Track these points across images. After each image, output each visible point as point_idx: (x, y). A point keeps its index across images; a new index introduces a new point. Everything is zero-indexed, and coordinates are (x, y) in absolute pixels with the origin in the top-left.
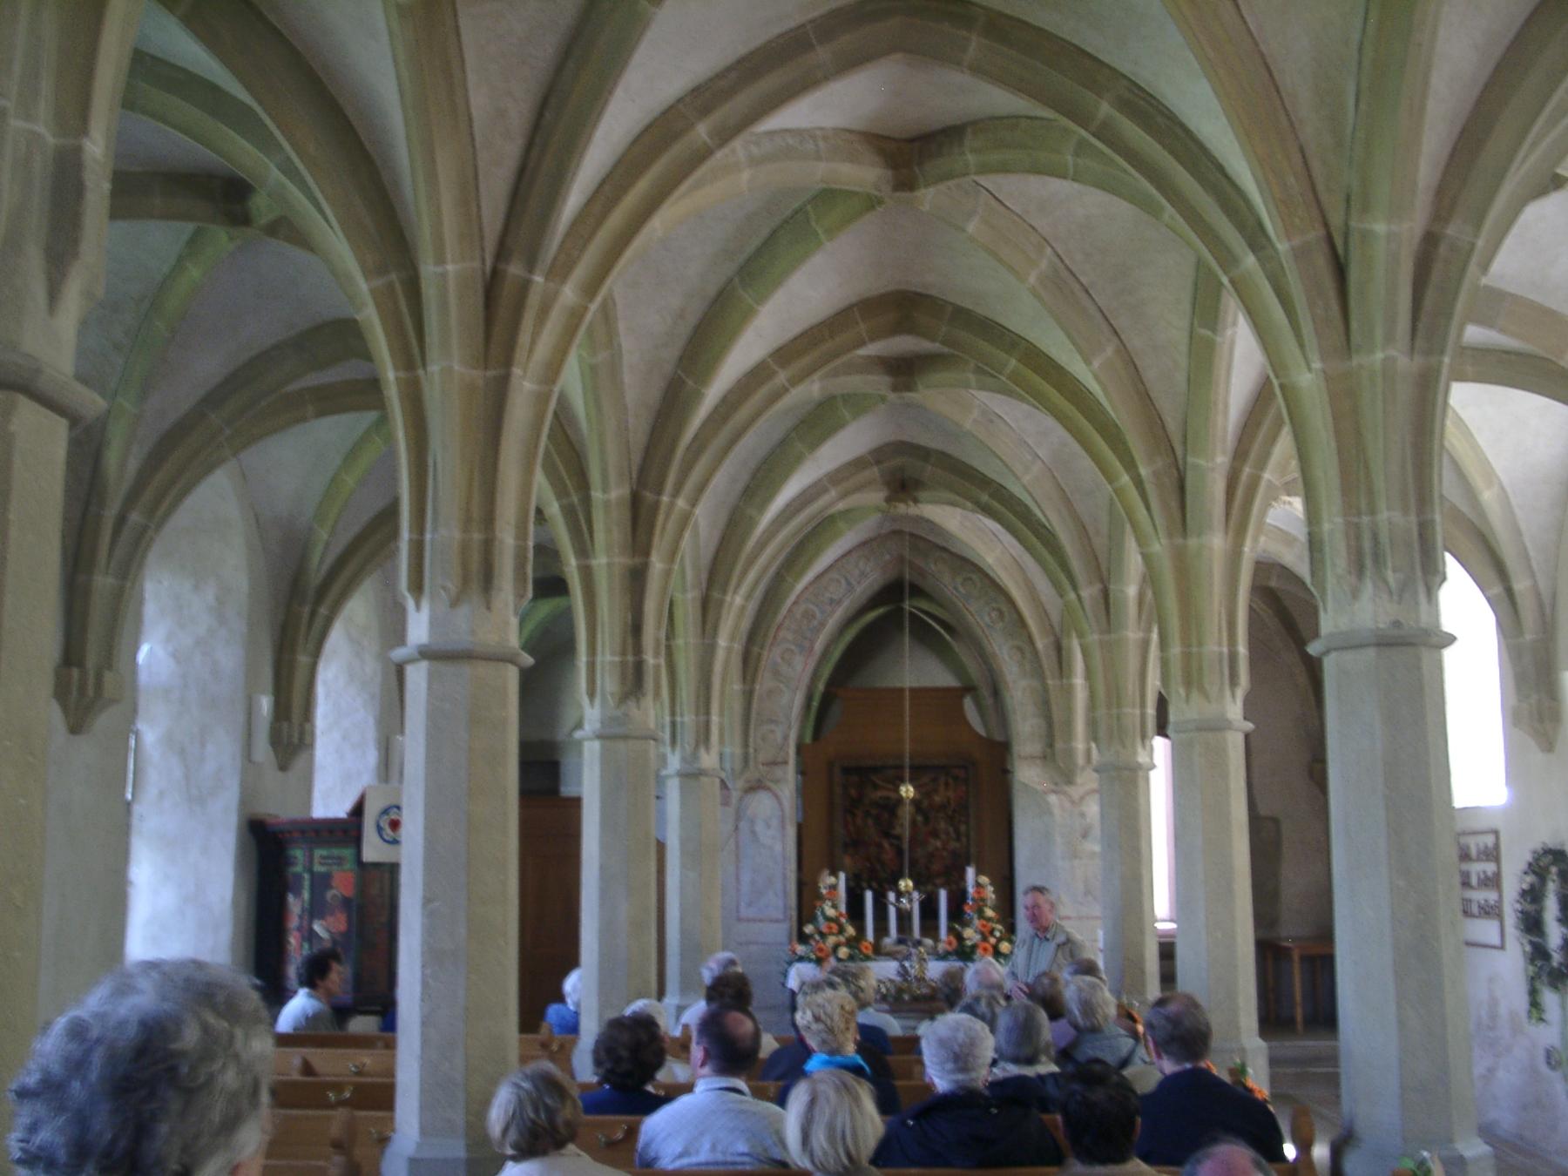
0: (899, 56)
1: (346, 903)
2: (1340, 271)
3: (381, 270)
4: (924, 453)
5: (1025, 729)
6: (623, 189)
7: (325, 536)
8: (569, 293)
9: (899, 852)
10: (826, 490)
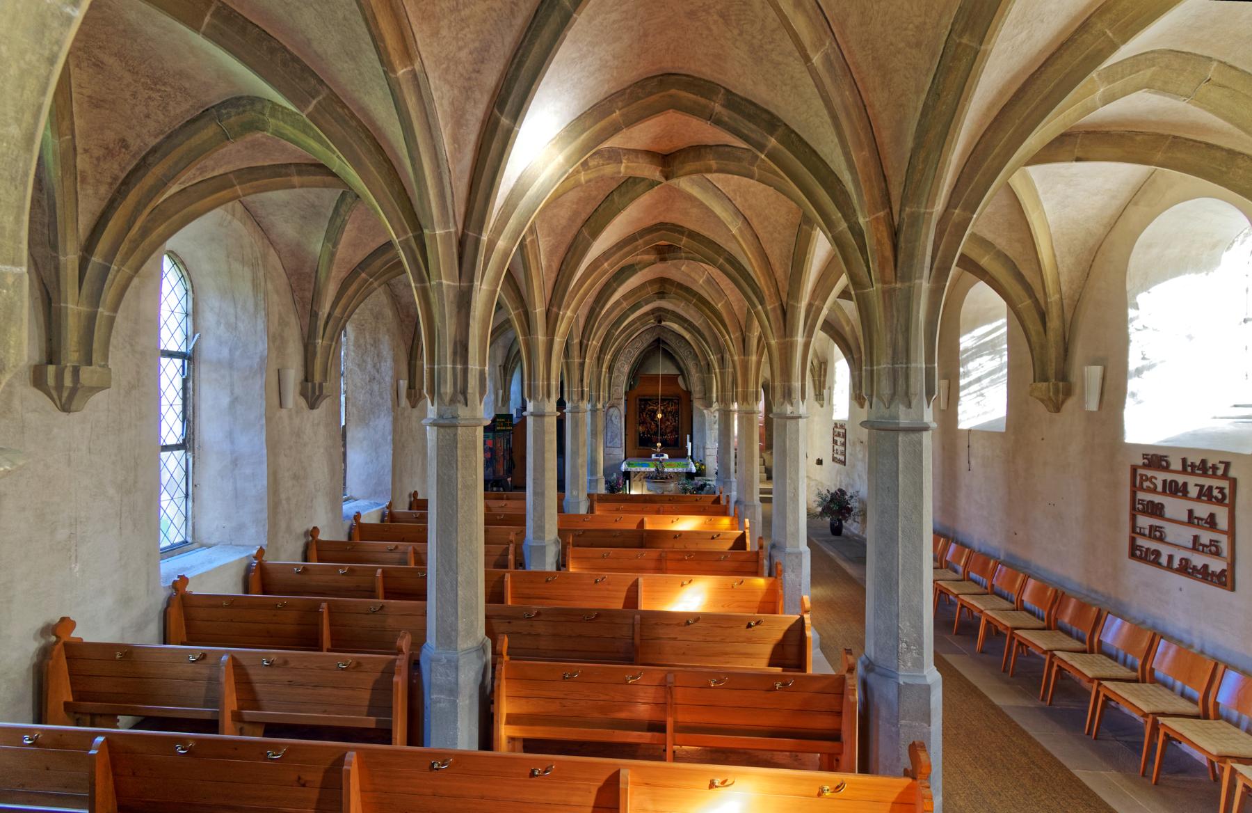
2: (784, 313)
3: (517, 308)
5: (696, 388)
6: (581, 286)
7: (444, 282)
8: (569, 313)
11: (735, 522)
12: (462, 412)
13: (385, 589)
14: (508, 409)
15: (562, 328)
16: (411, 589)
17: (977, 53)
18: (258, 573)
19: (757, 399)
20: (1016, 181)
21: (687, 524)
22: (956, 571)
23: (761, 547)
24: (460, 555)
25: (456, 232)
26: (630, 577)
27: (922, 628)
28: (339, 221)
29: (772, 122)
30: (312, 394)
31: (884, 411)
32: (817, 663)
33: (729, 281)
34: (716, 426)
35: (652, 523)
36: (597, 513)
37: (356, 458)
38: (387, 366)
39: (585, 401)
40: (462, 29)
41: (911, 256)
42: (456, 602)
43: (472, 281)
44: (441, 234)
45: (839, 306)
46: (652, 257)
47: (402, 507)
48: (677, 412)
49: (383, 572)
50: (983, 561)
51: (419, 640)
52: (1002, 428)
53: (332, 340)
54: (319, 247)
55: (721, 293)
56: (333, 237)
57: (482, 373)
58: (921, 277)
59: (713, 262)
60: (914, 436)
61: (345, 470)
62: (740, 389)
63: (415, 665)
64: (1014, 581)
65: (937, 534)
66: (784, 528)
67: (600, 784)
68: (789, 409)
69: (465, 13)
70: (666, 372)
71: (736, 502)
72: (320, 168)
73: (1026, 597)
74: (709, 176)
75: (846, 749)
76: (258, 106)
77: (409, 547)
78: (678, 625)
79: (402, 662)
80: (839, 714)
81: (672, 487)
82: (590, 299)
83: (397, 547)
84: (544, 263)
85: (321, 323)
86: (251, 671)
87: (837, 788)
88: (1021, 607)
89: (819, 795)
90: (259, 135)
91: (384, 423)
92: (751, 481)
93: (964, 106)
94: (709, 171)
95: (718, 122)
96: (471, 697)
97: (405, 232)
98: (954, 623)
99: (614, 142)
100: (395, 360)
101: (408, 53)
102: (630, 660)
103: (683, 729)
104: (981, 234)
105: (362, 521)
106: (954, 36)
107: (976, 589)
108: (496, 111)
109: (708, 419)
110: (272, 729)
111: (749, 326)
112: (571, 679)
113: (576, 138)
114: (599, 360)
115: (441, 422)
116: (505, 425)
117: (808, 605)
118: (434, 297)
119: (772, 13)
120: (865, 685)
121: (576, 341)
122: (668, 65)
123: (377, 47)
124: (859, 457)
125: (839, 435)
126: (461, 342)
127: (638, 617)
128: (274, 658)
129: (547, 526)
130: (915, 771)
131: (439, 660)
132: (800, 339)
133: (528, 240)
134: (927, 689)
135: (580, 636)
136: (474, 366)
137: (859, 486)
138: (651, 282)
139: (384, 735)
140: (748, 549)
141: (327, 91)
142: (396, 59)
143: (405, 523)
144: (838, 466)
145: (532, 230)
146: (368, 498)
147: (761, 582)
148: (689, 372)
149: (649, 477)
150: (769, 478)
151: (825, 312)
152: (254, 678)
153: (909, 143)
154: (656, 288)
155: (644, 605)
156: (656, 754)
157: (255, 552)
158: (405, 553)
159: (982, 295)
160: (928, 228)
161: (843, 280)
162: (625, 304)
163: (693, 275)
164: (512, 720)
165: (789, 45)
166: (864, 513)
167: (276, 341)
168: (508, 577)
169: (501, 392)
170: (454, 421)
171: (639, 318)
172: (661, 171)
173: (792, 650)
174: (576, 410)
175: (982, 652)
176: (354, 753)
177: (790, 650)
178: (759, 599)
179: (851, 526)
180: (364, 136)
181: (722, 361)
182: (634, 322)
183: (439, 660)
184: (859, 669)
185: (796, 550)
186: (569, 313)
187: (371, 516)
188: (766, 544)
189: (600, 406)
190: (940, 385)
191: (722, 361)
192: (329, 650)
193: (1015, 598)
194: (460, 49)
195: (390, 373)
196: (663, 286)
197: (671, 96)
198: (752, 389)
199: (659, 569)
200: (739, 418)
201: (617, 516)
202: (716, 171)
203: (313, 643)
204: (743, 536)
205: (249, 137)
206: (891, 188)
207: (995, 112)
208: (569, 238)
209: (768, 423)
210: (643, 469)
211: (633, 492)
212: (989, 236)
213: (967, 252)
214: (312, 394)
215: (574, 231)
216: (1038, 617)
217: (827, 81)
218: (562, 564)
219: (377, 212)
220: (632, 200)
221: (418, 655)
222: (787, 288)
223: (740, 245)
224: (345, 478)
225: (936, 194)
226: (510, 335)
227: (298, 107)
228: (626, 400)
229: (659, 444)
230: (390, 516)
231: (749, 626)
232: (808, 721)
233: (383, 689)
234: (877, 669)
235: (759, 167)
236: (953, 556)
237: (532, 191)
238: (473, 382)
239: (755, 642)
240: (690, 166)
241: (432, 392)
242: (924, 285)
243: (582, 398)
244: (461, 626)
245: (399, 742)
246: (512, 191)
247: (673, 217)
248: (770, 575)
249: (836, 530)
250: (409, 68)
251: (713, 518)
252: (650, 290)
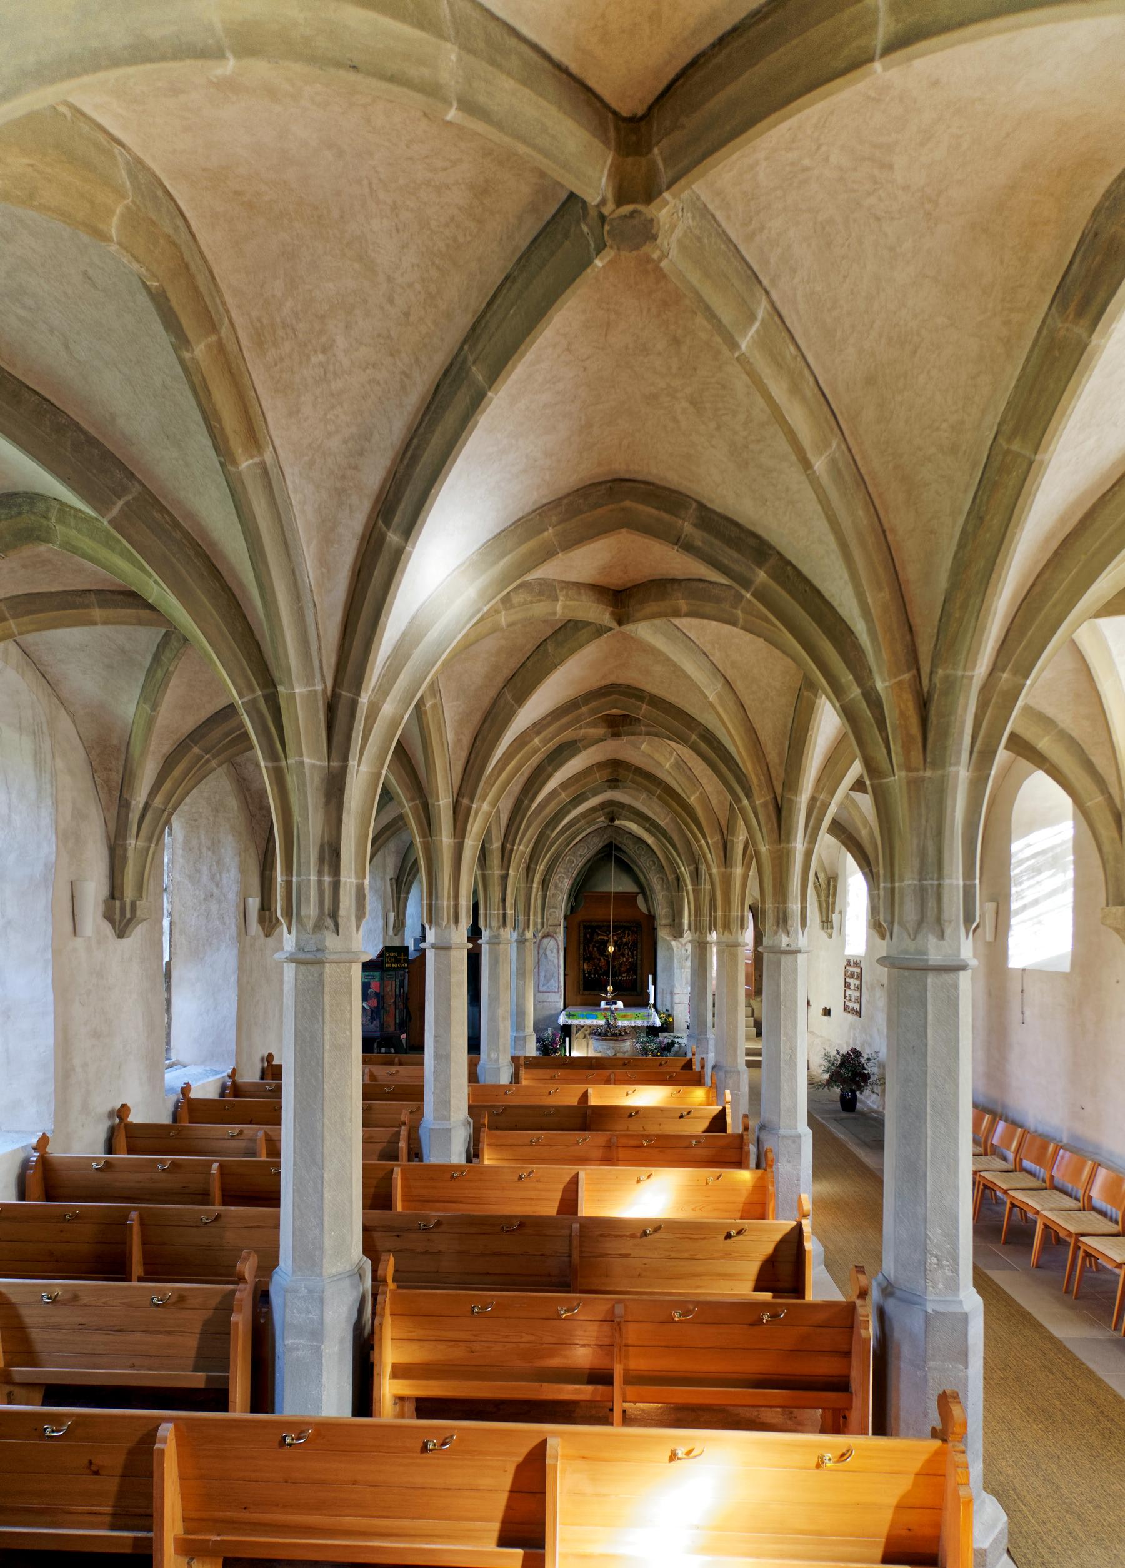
1: (377, 994)
2: (779, 810)
3: (412, 799)
5: (662, 913)
6: (503, 769)
7: (307, 760)
8: (485, 807)
9: (608, 962)
10: (579, 821)
11: (713, 1093)
12: (331, 941)
13: (223, 1190)
14: (403, 939)
15: (475, 829)
16: (259, 1191)
17: (1031, 463)
18: (39, 1174)
19: (743, 926)
20: (1084, 636)
21: (648, 1096)
22: (1005, 1159)
23: (746, 1129)
24: (327, 1144)
25: (324, 691)
26: (566, 1172)
27: (957, 1236)
28: (160, 674)
29: (760, 549)
30: (121, 914)
31: (910, 945)
32: (821, 1286)
33: (701, 762)
34: (689, 963)
35: (601, 1096)
36: (524, 1082)
37: (187, 1006)
38: (231, 879)
39: (509, 929)
40: (333, 407)
41: (944, 733)
42: (322, 1209)
43: (345, 759)
44: (303, 693)
45: (853, 801)
46: (600, 731)
47: (251, 1076)
48: (635, 944)
49: (221, 1166)
50: (1040, 1146)
51: (269, 1262)
52: (1066, 967)
53: (150, 840)
54: (131, 709)
55: (694, 781)
56: (152, 694)
57: (360, 889)
58: (958, 763)
59: (682, 739)
60: (947, 977)
61: (169, 1024)
62: (719, 913)
63: (262, 1297)
64: (1079, 1171)
65: (981, 1109)
66: (778, 1102)
67: (520, 1459)
68: (784, 941)
69: (337, 385)
70: (620, 889)
71: (714, 1067)
72: (131, 598)
73: (1096, 1193)
74: (677, 621)
75: (857, 1402)
76: (41, 506)
77: (259, 1132)
78: (633, 1236)
79: (244, 1294)
80: (848, 1354)
81: (627, 1046)
82: (516, 787)
83: (241, 1132)
84: (450, 737)
85: (134, 817)
86: (24, 1311)
87: (843, 1456)
88: (1088, 1206)
89: (818, 1466)
90: (42, 548)
91: (225, 957)
92: (735, 1040)
93: (1014, 534)
94: (677, 613)
95: (688, 547)
96: (342, 1341)
97: (253, 691)
98: (1002, 1228)
99: (547, 571)
100: (243, 871)
101: (254, 438)
102: (565, 1285)
103: (634, 1379)
104: (1037, 707)
105: (193, 1095)
106: (1001, 440)
107: (1032, 1182)
108: (380, 522)
109: (676, 956)
110: (56, 1394)
111: (731, 828)
112: (482, 1314)
113: (494, 563)
114: (529, 871)
115: (302, 956)
116: (398, 961)
117: (807, 1206)
118: (291, 781)
119: (760, 402)
120: (882, 1314)
121: (496, 845)
122: (620, 466)
123: (210, 429)
124: (877, 1002)
125: (852, 976)
126: (330, 845)
127: (576, 1226)
128: (58, 1291)
129: (453, 1102)
130: (945, 1431)
131: (296, 1291)
132: (799, 845)
133: (429, 704)
134: (965, 1318)
135: (498, 1254)
136: (348, 878)
137: (876, 1045)
138: (600, 765)
139: (217, 1398)
140: (730, 1131)
141: (138, 487)
142: (236, 445)
143: (251, 1101)
144: (851, 1017)
145: (434, 689)
146: (203, 1063)
147: (745, 1177)
148: (652, 889)
149: (596, 1033)
150: (759, 1034)
151: (833, 809)
152: (28, 1321)
153: (942, 580)
154: (606, 774)
155: (587, 1209)
156: (599, 1415)
157: (34, 1141)
158: (253, 1140)
159: (1040, 792)
160: (967, 698)
161: (857, 768)
162: (563, 795)
163: (657, 756)
164: (399, 1372)
165: (783, 446)
166: (882, 1081)
167: (69, 840)
168: (397, 1173)
169: (392, 915)
170: (319, 955)
171: (583, 815)
172: (613, 614)
173: (785, 1269)
174: (495, 942)
175: (1038, 1267)
176: (171, 1426)
177: (784, 1269)
178: (743, 1199)
179: (867, 1099)
180: (192, 553)
181: (696, 875)
182: (576, 820)
183: (296, 1291)
184: (875, 1294)
185: (793, 1132)
186: (485, 807)
187: (206, 1088)
188: (753, 1123)
189: (529, 935)
190: (984, 909)
191: (696, 875)
192: (140, 1280)
193: (1080, 1195)
194: (329, 435)
195: (235, 888)
196: (616, 772)
197: (623, 509)
198: (735, 912)
199: (609, 1158)
200: (718, 953)
201: (552, 1086)
202: (687, 615)
203: (112, 1265)
204: (723, 1112)
205: (28, 551)
206: (919, 641)
207: (1054, 545)
208: (486, 701)
209: (758, 958)
210: (588, 1022)
211: (575, 1054)
212: (1050, 711)
213: (1020, 731)
214: (121, 914)
215: (493, 693)
216: (1111, 1219)
217: (834, 495)
218: (473, 1154)
219: (211, 660)
220: (572, 652)
221: (267, 1284)
222: (783, 775)
223: (717, 713)
224: (168, 1035)
225: (977, 653)
226: (405, 836)
227: (95, 509)
228: (566, 928)
229: (610, 988)
230: (233, 1089)
231: (728, 1236)
232: (803, 1362)
233: (216, 1333)
234: (898, 1293)
235: (744, 611)
236: (1002, 1139)
237: (433, 635)
238: (347, 901)
239: (735, 1259)
240: (652, 607)
241: (288, 914)
242: (962, 773)
243: (504, 924)
244: (328, 1243)
245: (239, 1409)
246: (404, 635)
247: (630, 677)
248: (758, 1166)
249: (848, 1104)
250: (257, 460)
251: (683, 1088)
252: (599, 777)
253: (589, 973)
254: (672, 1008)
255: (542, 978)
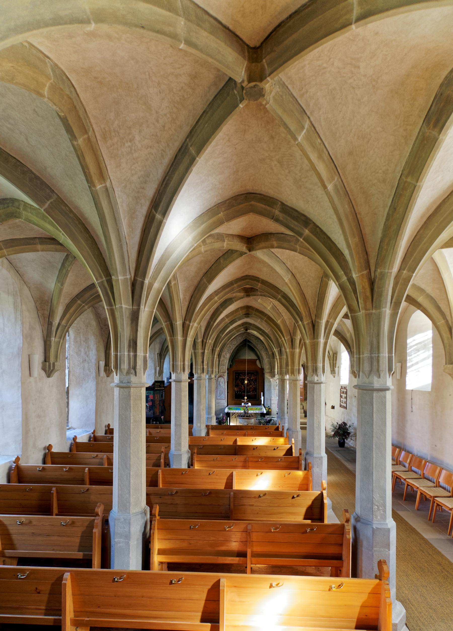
0: (251, 213)
2: (314, 326)
3: (166, 322)
4: (256, 279)
5: (266, 367)
6: (203, 310)
7: (123, 306)
8: (195, 325)
9: (245, 387)
10: (233, 330)
11: (287, 440)
12: (133, 379)
13: (90, 479)
14: (162, 378)
15: (191, 334)
16: (104, 479)
17: (415, 186)
18: (16, 473)
19: (299, 373)
20: (436, 256)
21: (261, 441)
22: (405, 466)
23: (300, 454)
24: (132, 460)
25: (131, 278)
26: (228, 471)
27: (385, 498)
28: (64, 271)
29: (306, 221)
30: (49, 368)
31: (366, 380)
32: (330, 517)
33: (282, 306)
34: (277, 388)
35: (242, 441)
36: (211, 436)
37: (75, 405)
38: (93, 354)
39: (205, 374)
40: (134, 164)
41: (380, 295)
42: (129, 486)
43: (139, 305)
44: (122, 279)
45: (344, 322)
46: (242, 294)
47: (101, 433)
48: (256, 380)
49: (89, 469)
50: (419, 461)
51: (108, 508)
52: (429, 389)
53: (60, 338)
54: (53, 285)
55: (279, 314)
56: (61, 279)
57: (145, 358)
58: (386, 307)
59: (275, 297)
60: (381, 393)
61: (68, 412)
62: (290, 368)
63: (106, 522)
64: (434, 471)
65: (395, 446)
66: (313, 443)
67: (209, 587)
68: (316, 379)
69: (136, 155)
70: (250, 358)
71: (287, 429)
72: (53, 241)
73: (441, 480)
74: (273, 250)
75: (345, 564)
76: (16, 204)
77: (104, 455)
78: (255, 497)
79: (98, 521)
80: (341, 545)
81: (253, 421)
82: (208, 317)
83: (97, 456)
84: (181, 296)
85: (54, 329)
86: (10, 528)
87: (339, 586)
88: (438, 485)
89: (329, 590)
90: (17, 220)
91: (91, 385)
92: (296, 418)
93: (408, 215)
94: (273, 247)
95: (277, 220)
96: (138, 540)
97: (102, 278)
98: (404, 494)
99: (220, 230)
100: (98, 351)
101: (102, 176)
102: (228, 517)
103: (255, 555)
104: (417, 284)
105: (78, 441)
106: (403, 177)
107: (415, 476)
108: (153, 210)
109: (272, 385)
110: (23, 561)
111: (295, 333)
112: (194, 529)
113: (199, 227)
114: (213, 351)
115: (122, 385)
116: (160, 387)
117: (325, 485)
118: (117, 314)
119: (306, 162)
120: (355, 529)
121: (200, 340)
122: (250, 188)
123: (85, 173)
124: (353, 403)
125: (343, 393)
126: (133, 340)
127: (232, 493)
128: (23, 520)
129: (182, 443)
130: (380, 576)
131: (119, 520)
132: (322, 340)
133: (173, 283)
134: (389, 530)
135: (200, 504)
136: (140, 353)
137: (353, 420)
138: (242, 308)
139: (87, 563)
140: (294, 455)
141: (56, 196)
142: (95, 179)
143: (101, 443)
144: (343, 409)
145: (175, 277)
146: (82, 428)
147: (300, 473)
148: (262, 358)
149: (240, 416)
150: (306, 416)
151: (335, 326)
152: (11, 532)
153: (379, 233)
154: (244, 311)
155: (236, 486)
156: (241, 569)
157: (14, 459)
158: (102, 459)
159: (419, 319)
160: (390, 281)
161: (345, 309)
162: (227, 320)
163: (264, 304)
164: (161, 552)
165: (315, 179)
166: (355, 435)
167: (28, 338)
168: (160, 472)
169: (158, 368)
170: (129, 384)
171: (235, 328)
172: (247, 247)
173: (316, 511)
174: (199, 379)
175: (418, 510)
176: (69, 574)
177: (316, 511)
178: (299, 483)
179: (349, 442)
180: (77, 223)
181: (280, 352)
182: (232, 330)
183: (119, 520)
184: (352, 521)
185: (319, 456)
186: (195, 325)
187: (83, 438)
188: (303, 452)
189: (213, 376)
190: (396, 366)
191: (280, 352)
192: (56, 515)
194: (133, 175)
195: (95, 357)
196: (248, 311)
197: (251, 205)
198: (296, 367)
199: (245, 466)
200: (289, 383)
201: (222, 437)
202: (276, 248)
203: (45, 509)
204: (291, 448)
205: (11, 222)
206: (370, 258)
207: (425, 219)
208: (196, 282)
209: (305, 386)
210: (237, 411)
211: (231, 424)
212: (423, 286)
213: (411, 294)
214: (49, 368)
215: (198, 279)
216: (447, 491)
217: (336, 199)
218: (191, 464)
219: (85, 266)
220: (230, 262)
221: (108, 517)
222: (315, 312)
223: (289, 287)
224: (68, 416)
225: (394, 263)
226: (163, 337)
227: (38, 205)
228: (228, 373)
229: (246, 398)
230: (94, 438)
231: (293, 497)
232: (323, 548)
233: (87, 536)
234: (362, 520)
235: (299, 246)
236: (403, 458)
237: (174, 256)
238: (140, 363)
239: (296, 506)
240: (263, 244)
241: (116, 368)
242: (387, 311)
243: (203, 372)
244: (132, 500)
245: (96, 567)
246: (163, 256)
247: (254, 272)
248: (305, 469)
249: (342, 444)
250: (103, 185)
251: (275, 438)
252: (241, 313)
253: (237, 391)
254: (271, 405)
255: (218, 393)
